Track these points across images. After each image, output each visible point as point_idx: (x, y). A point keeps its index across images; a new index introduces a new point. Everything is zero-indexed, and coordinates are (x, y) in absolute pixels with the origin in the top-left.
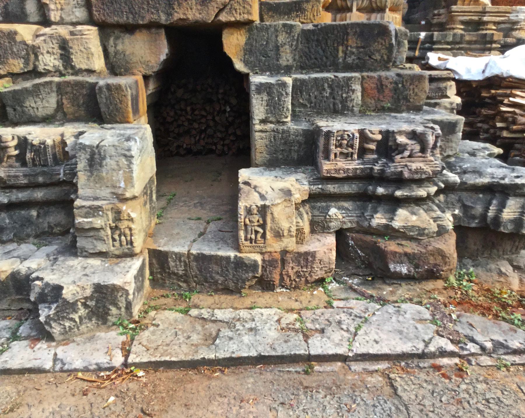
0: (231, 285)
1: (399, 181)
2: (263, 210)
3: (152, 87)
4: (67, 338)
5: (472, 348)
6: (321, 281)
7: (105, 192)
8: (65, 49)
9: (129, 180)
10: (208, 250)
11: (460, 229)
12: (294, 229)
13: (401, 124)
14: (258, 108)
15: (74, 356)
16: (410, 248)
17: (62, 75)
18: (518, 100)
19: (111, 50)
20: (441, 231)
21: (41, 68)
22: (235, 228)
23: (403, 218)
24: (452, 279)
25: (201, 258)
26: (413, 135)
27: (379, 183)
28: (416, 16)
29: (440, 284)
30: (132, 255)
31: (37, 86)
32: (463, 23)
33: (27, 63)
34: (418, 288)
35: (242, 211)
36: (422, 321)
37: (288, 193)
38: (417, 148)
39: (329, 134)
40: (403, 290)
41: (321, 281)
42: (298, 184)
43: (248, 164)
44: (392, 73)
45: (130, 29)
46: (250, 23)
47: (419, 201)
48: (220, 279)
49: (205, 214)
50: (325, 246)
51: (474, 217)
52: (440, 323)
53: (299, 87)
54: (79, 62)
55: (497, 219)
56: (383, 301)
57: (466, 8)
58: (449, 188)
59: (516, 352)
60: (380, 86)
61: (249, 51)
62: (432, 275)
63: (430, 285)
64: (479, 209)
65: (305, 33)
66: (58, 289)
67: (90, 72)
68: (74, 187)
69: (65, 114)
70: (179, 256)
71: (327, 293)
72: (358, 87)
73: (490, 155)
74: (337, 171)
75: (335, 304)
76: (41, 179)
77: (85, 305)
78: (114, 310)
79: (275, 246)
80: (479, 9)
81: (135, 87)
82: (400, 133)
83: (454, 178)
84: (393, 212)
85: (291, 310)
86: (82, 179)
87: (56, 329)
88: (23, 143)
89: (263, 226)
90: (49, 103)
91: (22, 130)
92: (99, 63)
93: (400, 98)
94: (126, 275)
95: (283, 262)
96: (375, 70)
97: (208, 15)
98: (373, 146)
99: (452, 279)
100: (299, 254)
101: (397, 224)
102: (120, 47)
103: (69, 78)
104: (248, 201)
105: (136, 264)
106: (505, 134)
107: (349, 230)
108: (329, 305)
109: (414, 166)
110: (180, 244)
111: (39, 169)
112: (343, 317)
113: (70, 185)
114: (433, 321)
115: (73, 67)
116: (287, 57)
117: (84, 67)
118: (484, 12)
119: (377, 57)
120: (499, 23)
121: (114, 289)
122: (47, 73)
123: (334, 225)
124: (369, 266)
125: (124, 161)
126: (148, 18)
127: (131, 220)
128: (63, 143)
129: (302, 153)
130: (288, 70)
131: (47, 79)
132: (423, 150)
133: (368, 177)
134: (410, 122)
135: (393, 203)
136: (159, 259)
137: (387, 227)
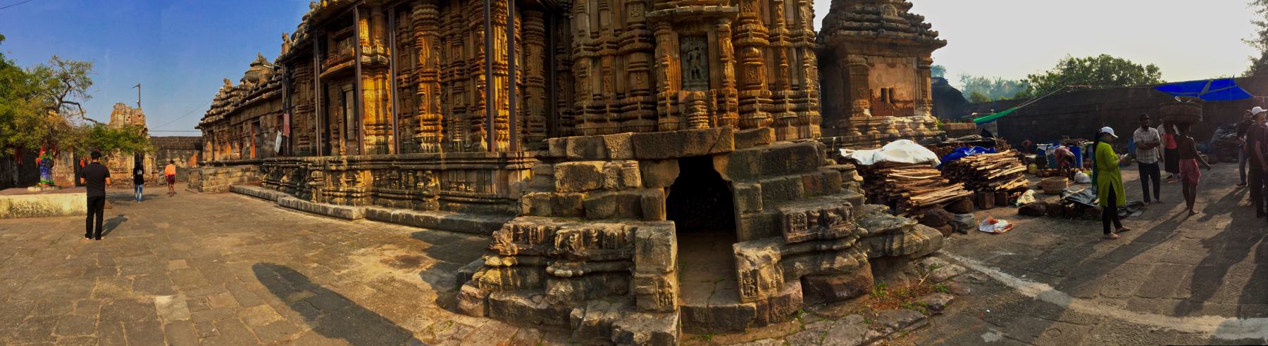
0: (738, 327)
1: (834, 239)
2: (755, 273)
5: (888, 330)
6: (795, 314)
7: (653, 268)
8: (620, 175)
13: (830, 205)
14: (741, 205)
16: (846, 279)
20: (862, 264)
23: (840, 261)
24: (874, 291)
25: (716, 310)
26: (837, 211)
27: (822, 242)
29: (867, 297)
30: (672, 311)
31: (604, 198)
34: (854, 303)
36: (859, 323)
37: (767, 259)
39: (788, 217)
40: (847, 307)
41: (795, 314)
42: (771, 251)
45: (657, 161)
46: (730, 152)
47: (847, 249)
48: (730, 323)
52: (869, 320)
53: (766, 188)
54: (628, 182)
56: (835, 318)
58: (863, 238)
59: (911, 324)
60: (814, 182)
61: (729, 169)
62: (862, 293)
63: (861, 300)
64: (880, 246)
68: (633, 264)
70: (701, 310)
71: (800, 320)
73: (884, 212)
75: (807, 327)
79: (763, 295)
81: (660, 193)
84: (834, 258)
85: (779, 338)
86: (638, 259)
88: (601, 234)
89: (755, 284)
90: (611, 207)
91: (599, 225)
93: (826, 187)
95: (771, 305)
97: (704, 151)
99: (874, 291)
101: (836, 266)
103: (623, 193)
104: (745, 268)
108: (803, 328)
109: (841, 229)
112: (812, 334)
113: (630, 260)
114: (866, 322)
116: (754, 169)
118: (868, 121)
122: (609, 189)
123: (799, 273)
124: (823, 296)
128: (624, 234)
129: (772, 230)
130: (756, 178)
131: (610, 193)
132: (844, 219)
133: (815, 240)
134: (834, 202)
135: (833, 253)
137: (830, 269)
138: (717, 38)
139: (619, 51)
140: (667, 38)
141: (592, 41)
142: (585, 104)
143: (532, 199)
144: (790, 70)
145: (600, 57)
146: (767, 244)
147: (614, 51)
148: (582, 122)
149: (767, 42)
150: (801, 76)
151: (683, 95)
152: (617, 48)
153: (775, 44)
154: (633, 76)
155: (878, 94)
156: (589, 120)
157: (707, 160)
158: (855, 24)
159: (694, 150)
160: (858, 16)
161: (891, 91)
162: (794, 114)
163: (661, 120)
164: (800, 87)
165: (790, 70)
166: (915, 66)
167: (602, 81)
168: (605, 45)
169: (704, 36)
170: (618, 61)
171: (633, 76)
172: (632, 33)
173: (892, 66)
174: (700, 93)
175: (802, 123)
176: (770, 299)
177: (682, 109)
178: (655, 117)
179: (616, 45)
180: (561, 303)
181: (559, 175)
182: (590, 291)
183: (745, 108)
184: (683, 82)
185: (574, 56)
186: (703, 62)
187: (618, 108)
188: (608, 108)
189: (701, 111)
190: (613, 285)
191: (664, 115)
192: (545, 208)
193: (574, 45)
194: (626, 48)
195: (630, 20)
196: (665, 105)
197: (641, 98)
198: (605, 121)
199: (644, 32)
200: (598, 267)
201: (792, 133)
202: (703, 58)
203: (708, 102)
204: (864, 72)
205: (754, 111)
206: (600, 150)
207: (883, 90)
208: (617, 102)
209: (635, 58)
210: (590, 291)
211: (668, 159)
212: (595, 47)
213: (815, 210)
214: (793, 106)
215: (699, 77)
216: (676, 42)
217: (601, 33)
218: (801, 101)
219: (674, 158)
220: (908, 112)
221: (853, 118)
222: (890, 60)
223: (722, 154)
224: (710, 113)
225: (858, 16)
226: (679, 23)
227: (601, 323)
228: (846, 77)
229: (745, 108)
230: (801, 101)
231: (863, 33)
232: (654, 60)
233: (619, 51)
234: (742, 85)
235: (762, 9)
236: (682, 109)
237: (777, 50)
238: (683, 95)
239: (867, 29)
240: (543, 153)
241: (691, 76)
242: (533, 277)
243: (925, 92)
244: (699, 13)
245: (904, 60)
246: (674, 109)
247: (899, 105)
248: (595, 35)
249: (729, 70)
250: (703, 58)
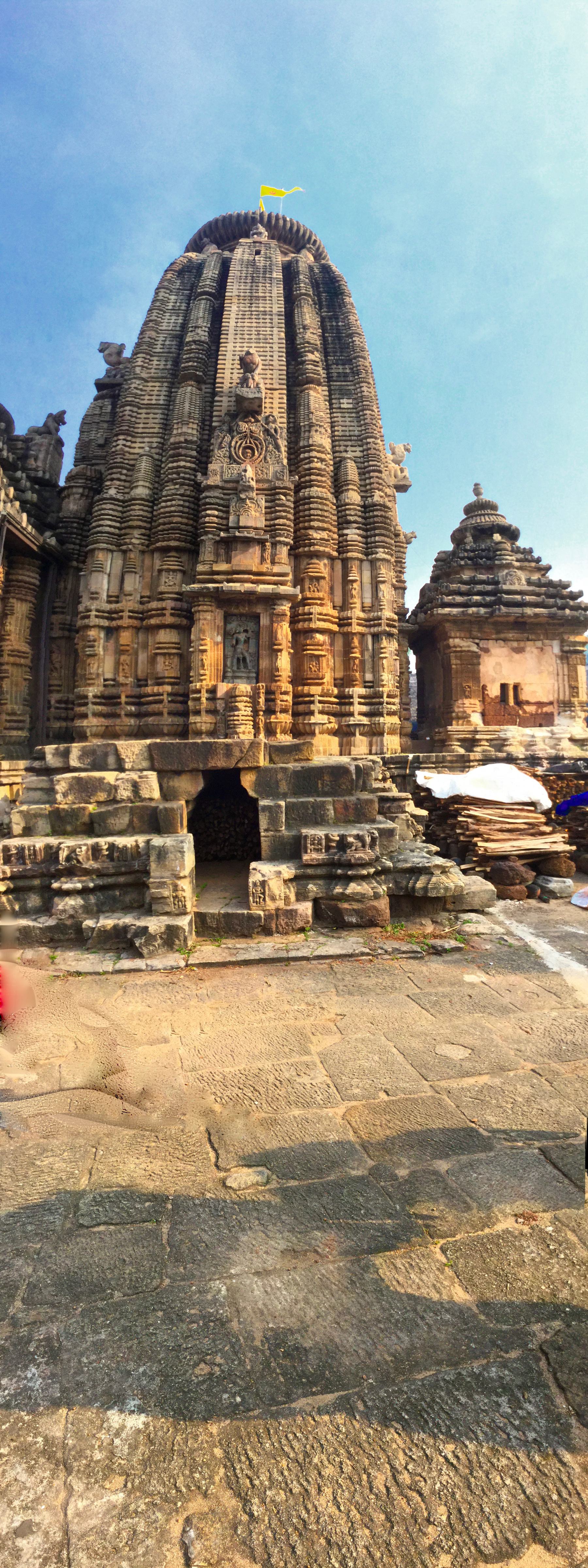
0: (246, 932)
1: (350, 865)
2: (263, 883)
3: (190, 807)
4: (151, 955)
7: (168, 874)
8: (135, 786)
9: (183, 866)
10: (230, 911)
11: (391, 896)
12: (283, 895)
13: (353, 831)
15: (157, 963)
16: (356, 906)
17: (132, 802)
18: (472, 812)
19: (165, 785)
20: (377, 896)
21: (119, 797)
22: (247, 895)
23: (353, 888)
25: (227, 915)
26: (358, 837)
27: (338, 867)
28: (421, 733)
32: (459, 740)
33: (109, 795)
35: (251, 885)
38: (360, 844)
39: (306, 837)
42: (287, 870)
43: (258, 858)
44: (353, 798)
45: (178, 773)
47: (364, 878)
49: (227, 894)
50: (306, 908)
51: (402, 888)
54: (145, 794)
55: (414, 887)
57: (460, 728)
58: (385, 871)
60: (346, 806)
61: (258, 785)
62: (372, 924)
64: (404, 883)
65: (296, 773)
66: (147, 928)
67: (151, 799)
68: (147, 873)
69: (134, 828)
70: (213, 915)
72: (331, 807)
74: (312, 860)
76: (123, 869)
77: (161, 937)
78: (177, 942)
79: (271, 906)
80: (472, 728)
81: (181, 807)
82: (350, 836)
83: (389, 864)
86: (153, 866)
87: (145, 951)
88: (112, 847)
89: (264, 893)
90: (123, 820)
91: (110, 839)
92: (157, 794)
94: (184, 922)
95: (277, 915)
96: (343, 796)
98: (334, 844)
100: (287, 911)
102: (171, 783)
105: (188, 918)
106: (462, 838)
107: (320, 898)
109: (357, 856)
110: (214, 908)
111: (122, 863)
115: (140, 797)
116: (284, 787)
117: (147, 796)
118: (476, 732)
119: (344, 787)
120: (491, 740)
121: (178, 928)
122: (122, 801)
123: (312, 895)
125: (179, 855)
126: (192, 766)
127: (183, 890)
128: (137, 846)
129: (290, 850)
130: (284, 796)
132: (364, 846)
133: (332, 864)
136: (201, 918)
137: (342, 894)
138: (272, 622)
139: (144, 622)
140: (208, 616)
141: (108, 607)
142: (92, 691)
143: (25, 815)
144: (362, 662)
145: (118, 628)
146: (283, 863)
147: (136, 623)
148: (85, 716)
149: (335, 628)
150: (376, 669)
151: (223, 688)
152: (142, 619)
153: (346, 629)
154: (160, 659)
155: (494, 691)
156: (95, 715)
157: (235, 774)
158: (459, 599)
159: (219, 762)
160: (464, 588)
161: (516, 687)
162: (365, 720)
163: (192, 719)
164: (375, 683)
165: (362, 662)
166: (556, 650)
167: (117, 664)
168: (126, 614)
169: (257, 617)
170: (141, 636)
171: (160, 659)
172: (163, 604)
173: (519, 650)
174: (244, 687)
175: (375, 733)
176: (277, 910)
177: (220, 705)
178: (185, 714)
179: (142, 616)
180: (72, 916)
181: (61, 787)
182: (103, 904)
183: (301, 708)
184: (225, 672)
185: (80, 623)
186: (252, 649)
187: (138, 700)
188: (123, 699)
189: (244, 710)
190: (128, 899)
191: (198, 713)
192: (43, 825)
193: (81, 608)
194: (153, 621)
195: (162, 588)
196: (199, 699)
197: (168, 688)
198: (118, 716)
199: (178, 604)
200: (110, 880)
201: (361, 745)
202: (252, 642)
203: (254, 698)
204: (472, 662)
205: (312, 713)
206: (111, 760)
207: (504, 687)
208: (137, 691)
209: (164, 636)
210: (103, 904)
211: (191, 771)
212: (111, 615)
213: (336, 834)
214: (364, 708)
215: (246, 667)
216: (220, 622)
217: (123, 598)
218: (374, 701)
219: (197, 770)
220: (544, 719)
221: (454, 727)
222: (515, 644)
223: (250, 769)
224: (255, 713)
225: (464, 588)
226: (225, 601)
227: (115, 927)
228: (447, 668)
229: (301, 708)
230: (374, 701)
231: (472, 610)
232: (190, 642)
233: (144, 622)
234: (299, 678)
235: (332, 588)
236: (220, 705)
237: (347, 637)
238: (223, 688)
239: (478, 605)
240: (37, 764)
241: (237, 663)
242: (34, 901)
243: (574, 690)
244: (252, 593)
245: (539, 644)
246: (211, 706)
247: (528, 708)
248: (113, 599)
249: (284, 662)
250: (252, 642)
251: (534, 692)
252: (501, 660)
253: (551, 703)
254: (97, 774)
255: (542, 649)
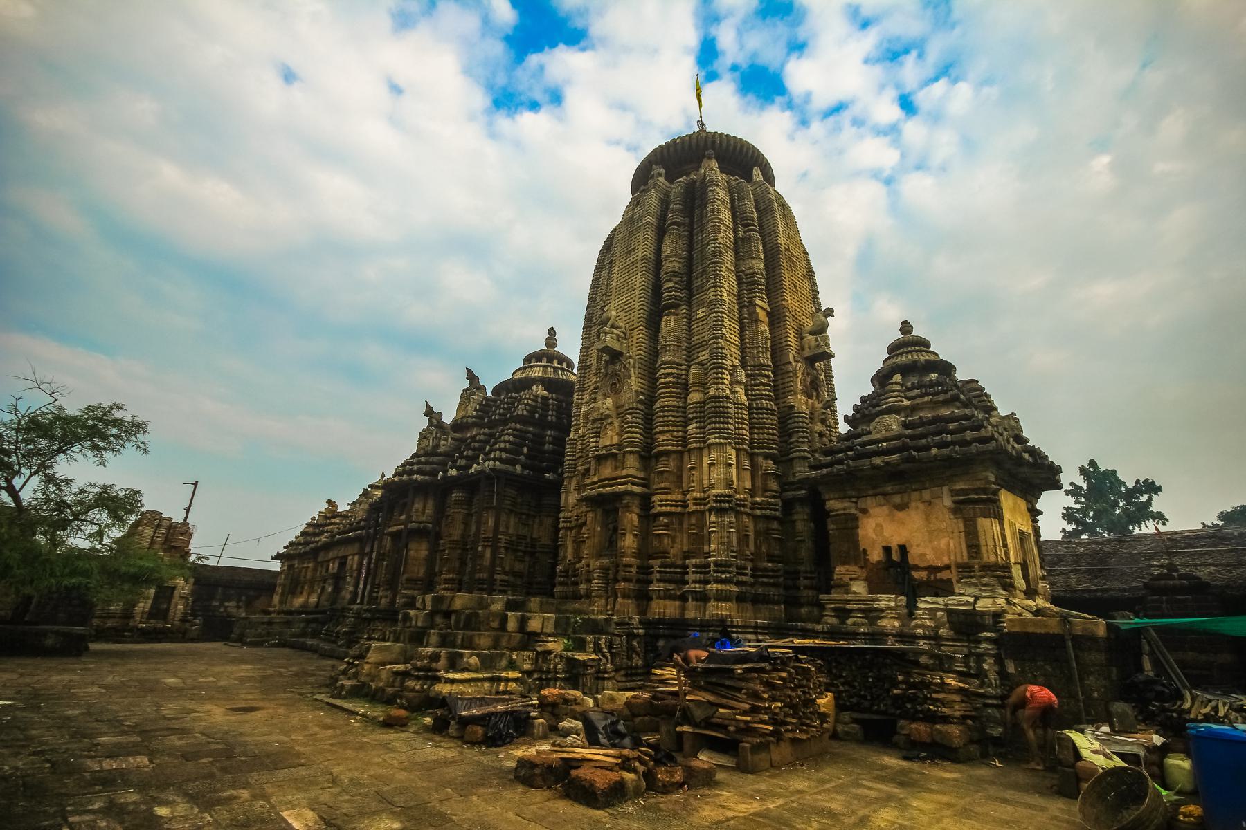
155: (876, 556)
173: (902, 507)
204: (850, 524)
207: (887, 550)
251: (923, 555)
252: (880, 520)
253: (948, 567)
254: (301, 640)
255: (930, 503)
